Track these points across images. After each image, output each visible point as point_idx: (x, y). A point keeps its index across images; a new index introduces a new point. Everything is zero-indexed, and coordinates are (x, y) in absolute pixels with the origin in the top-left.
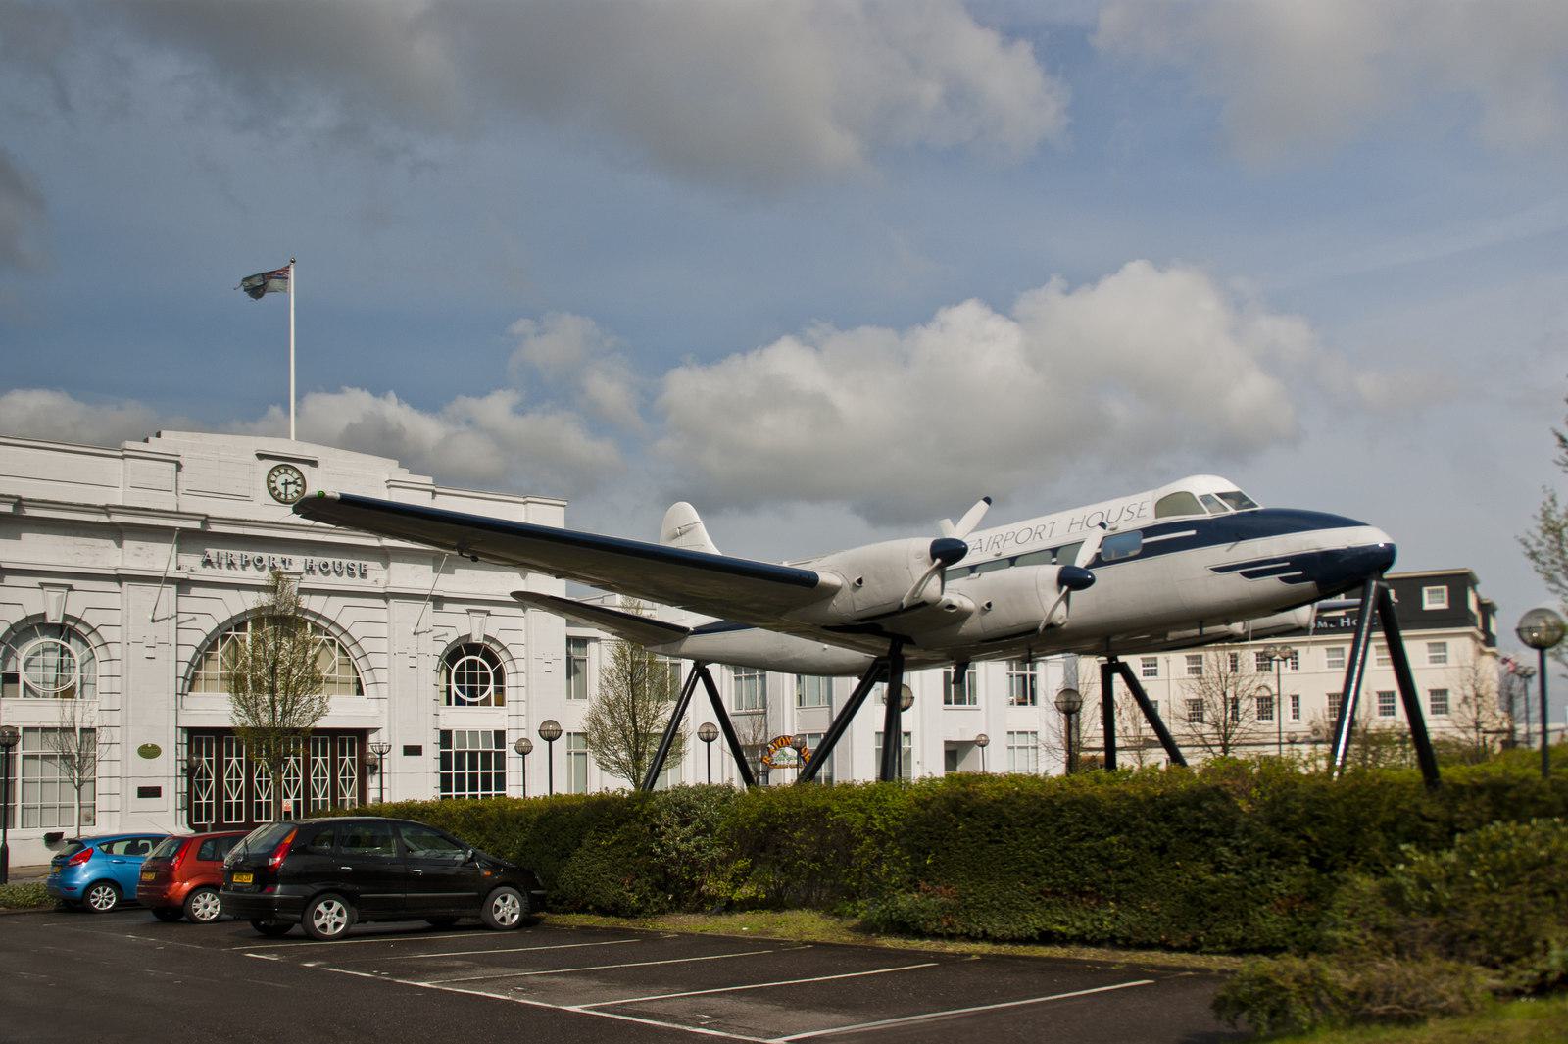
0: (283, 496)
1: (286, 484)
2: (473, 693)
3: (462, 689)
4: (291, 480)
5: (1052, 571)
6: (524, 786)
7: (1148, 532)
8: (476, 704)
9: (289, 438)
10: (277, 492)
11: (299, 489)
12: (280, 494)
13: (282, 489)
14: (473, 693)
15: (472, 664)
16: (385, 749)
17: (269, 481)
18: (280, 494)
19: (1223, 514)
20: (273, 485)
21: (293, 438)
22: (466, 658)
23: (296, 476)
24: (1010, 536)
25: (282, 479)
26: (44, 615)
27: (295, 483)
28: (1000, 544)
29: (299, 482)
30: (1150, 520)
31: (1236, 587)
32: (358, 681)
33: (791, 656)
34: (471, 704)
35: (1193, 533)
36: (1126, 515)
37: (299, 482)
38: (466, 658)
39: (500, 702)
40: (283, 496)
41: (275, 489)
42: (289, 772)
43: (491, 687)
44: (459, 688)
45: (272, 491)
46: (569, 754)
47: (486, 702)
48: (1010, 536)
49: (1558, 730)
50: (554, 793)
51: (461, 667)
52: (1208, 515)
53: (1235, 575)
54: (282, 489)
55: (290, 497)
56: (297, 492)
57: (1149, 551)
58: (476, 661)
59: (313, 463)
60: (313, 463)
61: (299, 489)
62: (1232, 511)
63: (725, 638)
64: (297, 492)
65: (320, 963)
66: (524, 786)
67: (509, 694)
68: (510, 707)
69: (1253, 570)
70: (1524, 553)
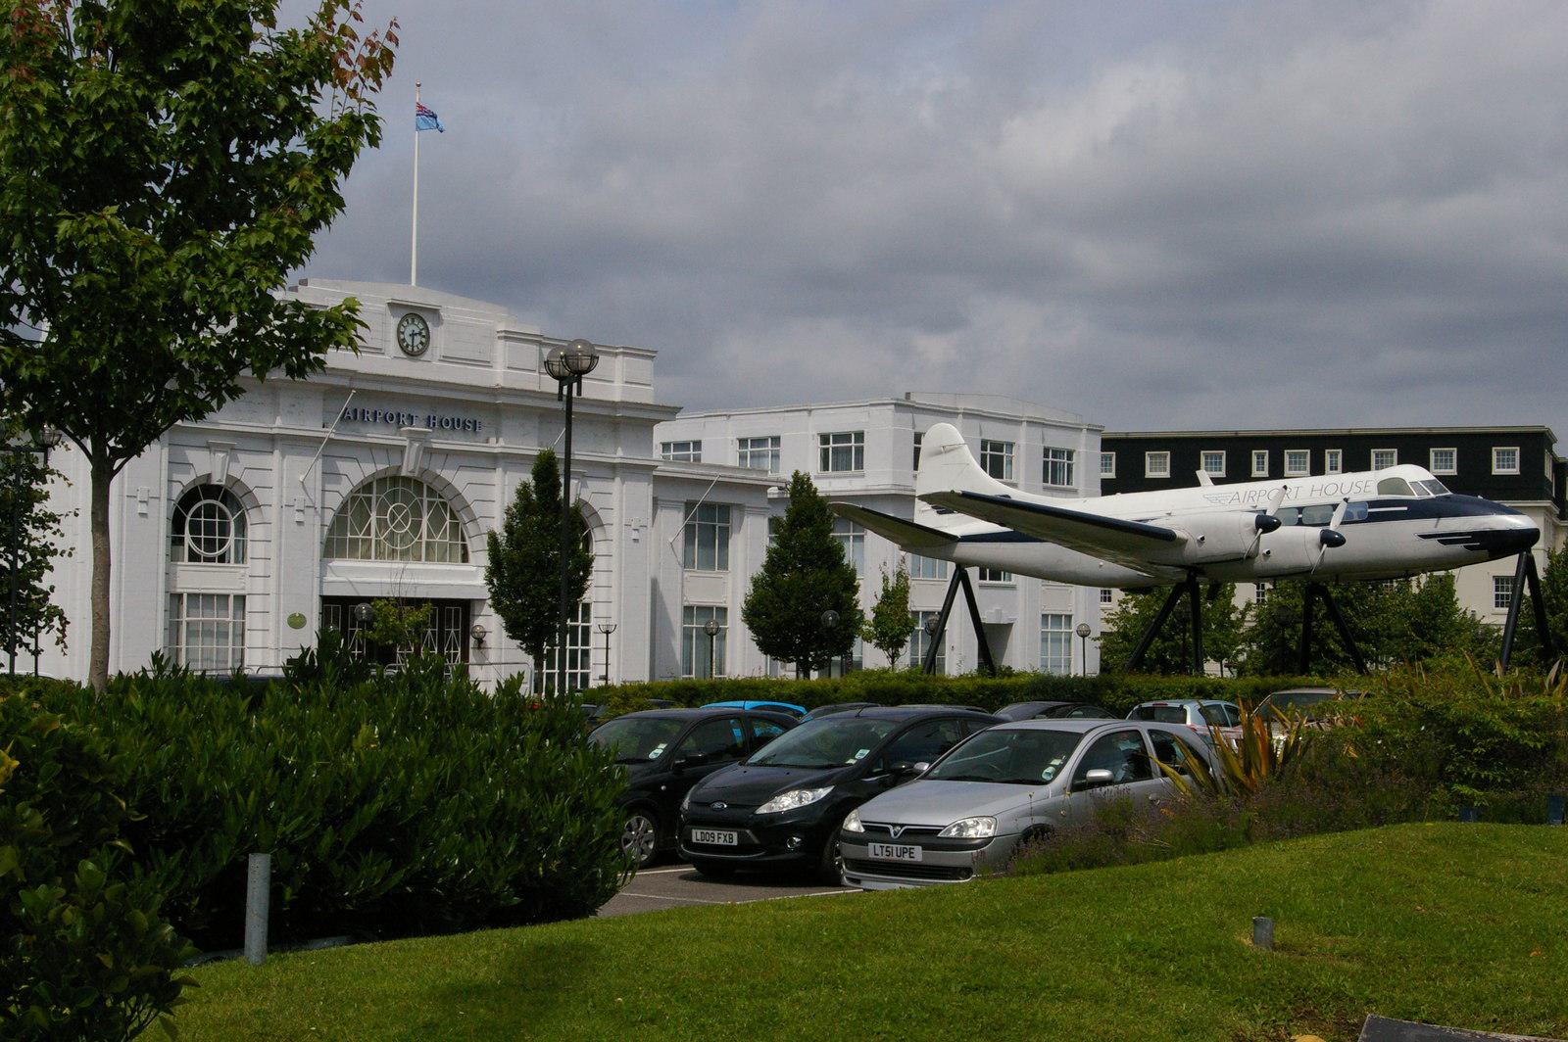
0: (410, 348)
1: (413, 335)
2: (210, 545)
3: (197, 541)
4: (417, 331)
5: (1316, 532)
6: (607, 664)
7: (1373, 504)
8: (212, 560)
10: (405, 344)
11: (424, 340)
12: (407, 346)
13: (409, 340)
14: (210, 545)
15: (210, 511)
17: (399, 332)
19: (1426, 497)
20: (402, 336)
21: (413, 284)
23: (421, 326)
24: (1263, 493)
25: (408, 331)
26: (209, 476)
27: (420, 333)
28: (1255, 498)
29: (424, 332)
30: (1374, 496)
31: (1433, 547)
33: (1067, 569)
34: (207, 560)
35: (1406, 509)
36: (1357, 490)
37: (424, 332)
39: (241, 558)
40: (410, 348)
41: (404, 340)
43: (232, 538)
44: (193, 539)
45: (401, 341)
46: (1044, 640)
48: (1263, 493)
50: (112, 671)
51: (197, 514)
52: (1416, 497)
53: (1434, 541)
54: (409, 340)
55: (416, 349)
57: (1373, 518)
58: (215, 506)
59: (298, 146)
60: (298, 146)
61: (424, 340)
62: (1432, 495)
63: (996, 548)
64: (421, 343)
65: (690, 792)
66: (607, 664)
67: (253, 550)
68: (254, 566)
69: (1446, 539)
70: (389, 74)
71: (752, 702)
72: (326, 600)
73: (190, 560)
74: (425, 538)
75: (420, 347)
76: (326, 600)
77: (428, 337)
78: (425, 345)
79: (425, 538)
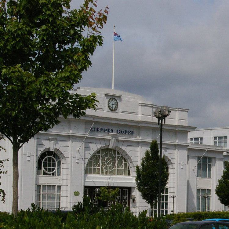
1: (113, 104)
2: (50, 170)
3: (45, 169)
4: (114, 103)
6: (173, 207)
8: (50, 175)
9: (111, 87)
10: (110, 107)
11: (116, 106)
13: (111, 106)
14: (50, 170)
15: (50, 159)
16: (175, 196)
18: (111, 108)
20: (109, 105)
21: (113, 88)
22: (48, 156)
23: (115, 102)
25: (111, 103)
32: (129, 171)
34: (49, 174)
38: (48, 156)
39: (59, 174)
40: (112, 109)
41: (110, 106)
42: (117, 201)
45: (109, 106)
47: (53, 174)
49: (72, 160)
50: (19, 209)
51: (45, 160)
54: (111, 106)
55: (114, 109)
56: (115, 107)
58: (51, 158)
61: (116, 106)
64: (115, 107)
67: (63, 171)
68: (63, 177)
70: (105, 23)
71: (218, 219)
72: (86, 187)
73: (43, 175)
74: (116, 168)
75: (115, 108)
76: (86, 187)
77: (117, 105)
78: (117, 108)
79: (116, 168)
